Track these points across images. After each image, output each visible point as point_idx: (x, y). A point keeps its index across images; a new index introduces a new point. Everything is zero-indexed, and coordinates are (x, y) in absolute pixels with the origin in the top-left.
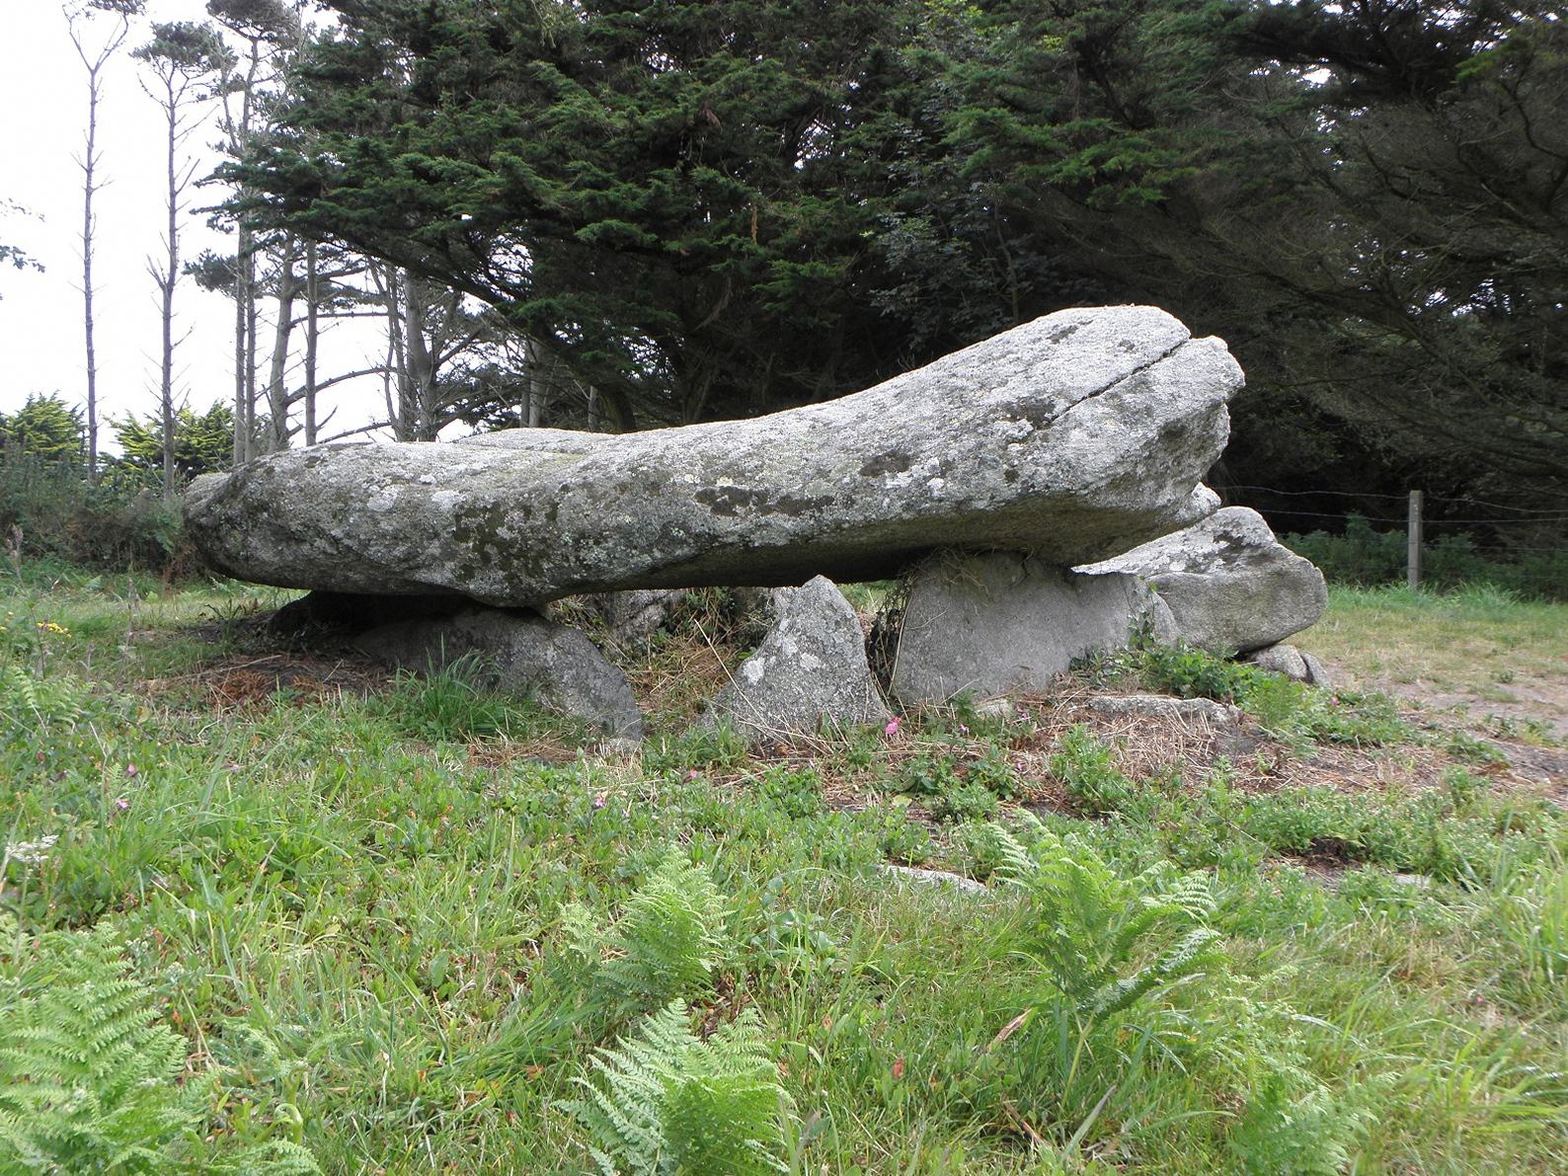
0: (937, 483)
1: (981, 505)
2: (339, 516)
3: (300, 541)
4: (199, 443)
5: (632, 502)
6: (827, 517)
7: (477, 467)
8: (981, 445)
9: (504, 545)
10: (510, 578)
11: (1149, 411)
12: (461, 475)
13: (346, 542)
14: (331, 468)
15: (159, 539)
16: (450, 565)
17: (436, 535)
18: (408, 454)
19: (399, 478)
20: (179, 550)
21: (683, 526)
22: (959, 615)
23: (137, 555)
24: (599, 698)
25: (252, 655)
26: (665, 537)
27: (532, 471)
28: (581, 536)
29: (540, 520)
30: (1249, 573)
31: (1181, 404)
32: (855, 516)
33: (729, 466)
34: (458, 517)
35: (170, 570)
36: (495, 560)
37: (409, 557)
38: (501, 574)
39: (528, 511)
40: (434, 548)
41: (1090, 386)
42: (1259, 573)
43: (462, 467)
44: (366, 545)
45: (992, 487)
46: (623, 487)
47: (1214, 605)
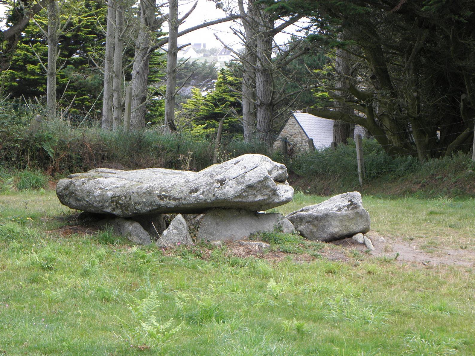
0: (201, 196)
1: (209, 201)
2: (88, 196)
3: (80, 201)
4: (80, 21)
5: (146, 196)
6: (181, 202)
7: (118, 186)
8: (210, 188)
9: (121, 204)
10: (122, 211)
11: (243, 182)
12: (114, 188)
13: (90, 202)
14: (87, 185)
15: (46, 148)
16: (110, 208)
17: (107, 201)
18: (104, 182)
19: (101, 188)
20: (58, 155)
21: (154, 202)
22: (215, 223)
23: (32, 157)
24: (141, 238)
25: (71, 226)
26: (151, 205)
27: (129, 187)
28: (135, 203)
29: (128, 199)
30: (350, 212)
31: (251, 181)
32: (185, 202)
33: (165, 190)
34: (112, 198)
35: (52, 167)
36: (119, 207)
37: (102, 206)
38: (121, 210)
39: (126, 197)
40: (107, 204)
41: (234, 176)
42: (353, 212)
43: (115, 186)
44: (93, 203)
45: (210, 198)
46: (144, 193)
47: (341, 221)
